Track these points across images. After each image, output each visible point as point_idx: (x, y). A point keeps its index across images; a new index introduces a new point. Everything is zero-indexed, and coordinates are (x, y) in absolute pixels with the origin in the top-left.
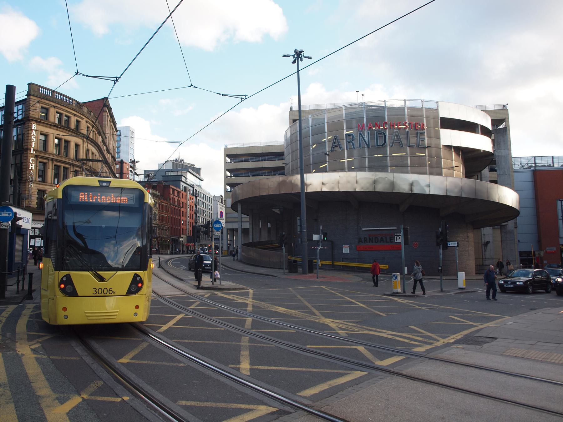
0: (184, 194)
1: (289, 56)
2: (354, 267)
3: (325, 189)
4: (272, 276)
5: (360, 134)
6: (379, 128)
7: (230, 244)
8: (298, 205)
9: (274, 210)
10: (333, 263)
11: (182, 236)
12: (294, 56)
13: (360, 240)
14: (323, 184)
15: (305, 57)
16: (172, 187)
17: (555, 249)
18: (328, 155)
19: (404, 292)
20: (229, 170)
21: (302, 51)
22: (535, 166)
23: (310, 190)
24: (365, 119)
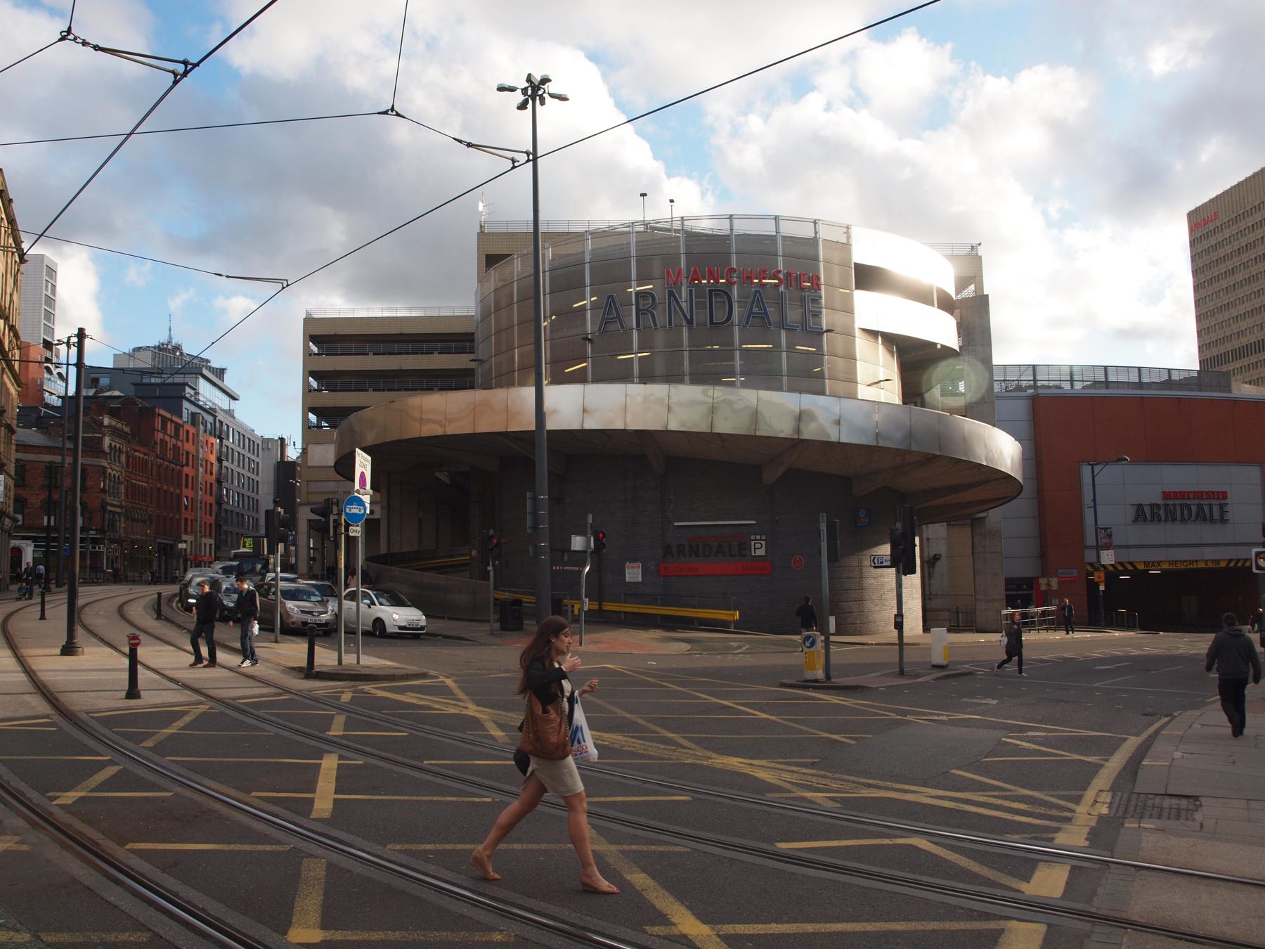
0: (192, 430)
1: (512, 89)
2: (654, 616)
3: (590, 424)
4: (462, 639)
5: (671, 294)
6: (717, 281)
7: (313, 559)
8: (529, 464)
9: (437, 474)
10: (600, 605)
11: (184, 537)
12: (524, 91)
13: (667, 551)
14: (585, 411)
15: (552, 96)
16: (162, 412)
17: (1075, 573)
18: (590, 341)
19: (828, 677)
20: (313, 374)
21: (545, 80)
22: (1035, 387)
23: (551, 425)
24: (683, 257)
